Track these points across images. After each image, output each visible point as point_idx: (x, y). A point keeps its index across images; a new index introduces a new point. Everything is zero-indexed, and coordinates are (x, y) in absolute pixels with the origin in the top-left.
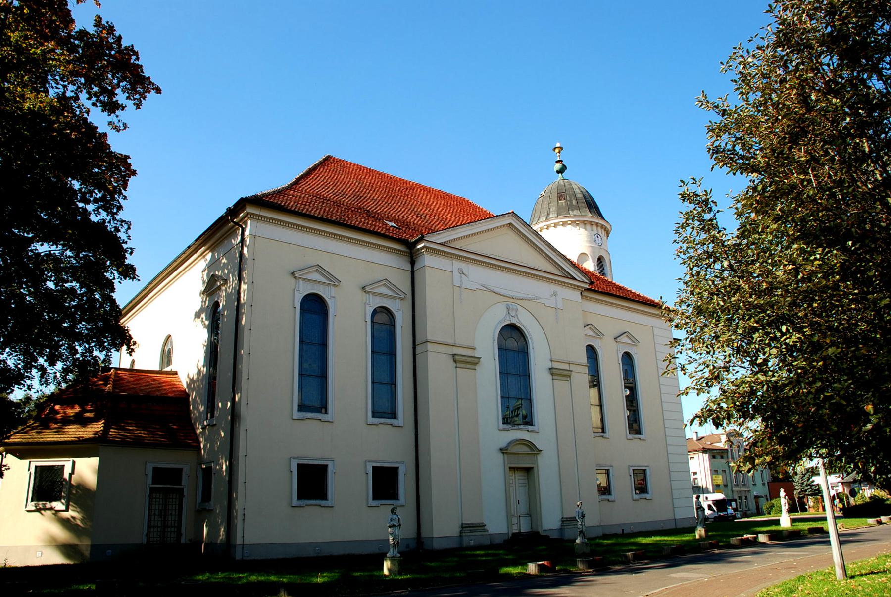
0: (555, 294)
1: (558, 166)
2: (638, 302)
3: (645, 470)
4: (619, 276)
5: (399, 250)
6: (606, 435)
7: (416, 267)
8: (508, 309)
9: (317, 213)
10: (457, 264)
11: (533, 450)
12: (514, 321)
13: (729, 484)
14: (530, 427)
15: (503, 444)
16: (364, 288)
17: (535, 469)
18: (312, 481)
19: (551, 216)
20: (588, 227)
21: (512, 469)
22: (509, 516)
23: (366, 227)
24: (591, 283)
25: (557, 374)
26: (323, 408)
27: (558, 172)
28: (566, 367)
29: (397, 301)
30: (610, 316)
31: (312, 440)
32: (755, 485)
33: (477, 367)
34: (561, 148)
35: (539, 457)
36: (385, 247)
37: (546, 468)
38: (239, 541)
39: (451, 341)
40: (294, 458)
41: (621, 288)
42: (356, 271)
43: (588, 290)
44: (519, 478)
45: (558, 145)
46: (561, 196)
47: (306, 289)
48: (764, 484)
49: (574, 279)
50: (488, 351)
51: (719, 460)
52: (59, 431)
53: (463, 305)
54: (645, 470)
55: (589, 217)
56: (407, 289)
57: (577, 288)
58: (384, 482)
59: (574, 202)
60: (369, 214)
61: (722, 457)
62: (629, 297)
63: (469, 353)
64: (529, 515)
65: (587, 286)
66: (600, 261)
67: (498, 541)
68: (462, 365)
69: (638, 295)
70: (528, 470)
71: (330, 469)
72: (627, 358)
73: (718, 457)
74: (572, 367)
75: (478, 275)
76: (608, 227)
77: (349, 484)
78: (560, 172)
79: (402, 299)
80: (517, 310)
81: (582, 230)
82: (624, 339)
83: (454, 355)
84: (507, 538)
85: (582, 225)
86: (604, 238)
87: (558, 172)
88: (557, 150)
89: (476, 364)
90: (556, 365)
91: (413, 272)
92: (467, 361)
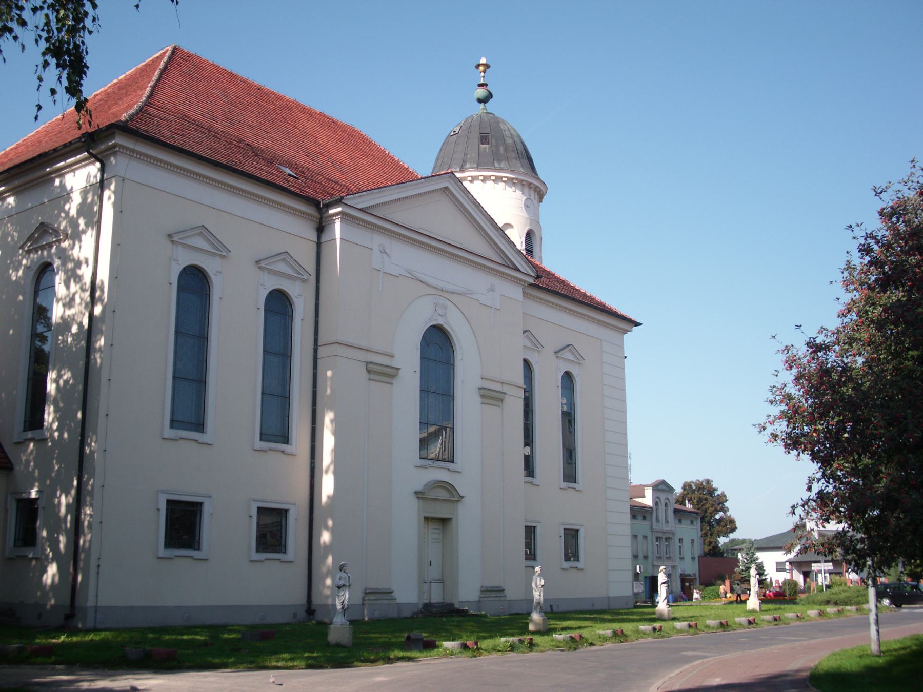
0: (492, 289)
1: (481, 92)
2: (588, 305)
3: (577, 531)
4: (551, 260)
5: (304, 213)
6: (535, 481)
7: (323, 239)
8: (436, 305)
9: (205, 154)
10: (378, 240)
11: (452, 494)
12: (440, 321)
13: (650, 555)
14: (450, 465)
15: (419, 487)
16: (258, 262)
17: (454, 521)
18: (183, 524)
19: (468, 165)
20: (526, 190)
21: (427, 519)
22: (423, 581)
23: (264, 176)
24: (538, 277)
25: (491, 396)
26: (199, 426)
27: (480, 101)
28: (497, 387)
29: (298, 283)
30: (556, 321)
31: (184, 469)
32: (682, 558)
33: (394, 381)
34: (487, 66)
35: (459, 505)
36: (290, 207)
37: (468, 519)
38: (91, 603)
39: (363, 344)
40: (163, 492)
41: (563, 282)
42: (251, 238)
43: (531, 285)
44: (433, 531)
45: (483, 61)
46: (484, 139)
47: (188, 259)
48: (693, 558)
49: (517, 270)
50: (408, 360)
51: (639, 522)
52: (851, 481)
53: (374, 290)
54: (577, 531)
55: (520, 174)
56: (311, 267)
57: (518, 281)
58: (271, 530)
59: (502, 149)
60: (256, 153)
61: (644, 518)
62: (577, 296)
63: (385, 361)
64: (441, 581)
65: (531, 281)
66: (529, 235)
67: (407, 613)
68: (377, 377)
69: (584, 295)
70: (444, 521)
71: (207, 510)
72: (568, 377)
73: (640, 517)
74: (506, 389)
75: (404, 257)
76: (543, 189)
77: (228, 530)
78: (483, 101)
79: (304, 281)
80: (445, 307)
81: (519, 193)
82: (567, 354)
83: (367, 363)
84: (415, 610)
85: (520, 187)
86: (536, 202)
87: (480, 101)
88: (481, 68)
89: (393, 376)
90: (488, 385)
91: (319, 244)
92: (383, 373)
